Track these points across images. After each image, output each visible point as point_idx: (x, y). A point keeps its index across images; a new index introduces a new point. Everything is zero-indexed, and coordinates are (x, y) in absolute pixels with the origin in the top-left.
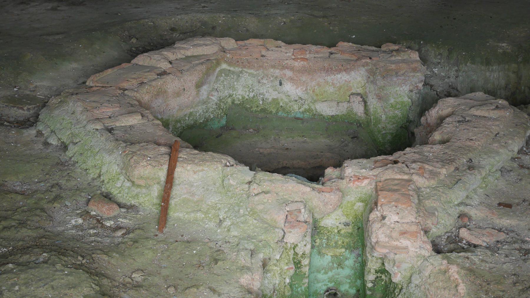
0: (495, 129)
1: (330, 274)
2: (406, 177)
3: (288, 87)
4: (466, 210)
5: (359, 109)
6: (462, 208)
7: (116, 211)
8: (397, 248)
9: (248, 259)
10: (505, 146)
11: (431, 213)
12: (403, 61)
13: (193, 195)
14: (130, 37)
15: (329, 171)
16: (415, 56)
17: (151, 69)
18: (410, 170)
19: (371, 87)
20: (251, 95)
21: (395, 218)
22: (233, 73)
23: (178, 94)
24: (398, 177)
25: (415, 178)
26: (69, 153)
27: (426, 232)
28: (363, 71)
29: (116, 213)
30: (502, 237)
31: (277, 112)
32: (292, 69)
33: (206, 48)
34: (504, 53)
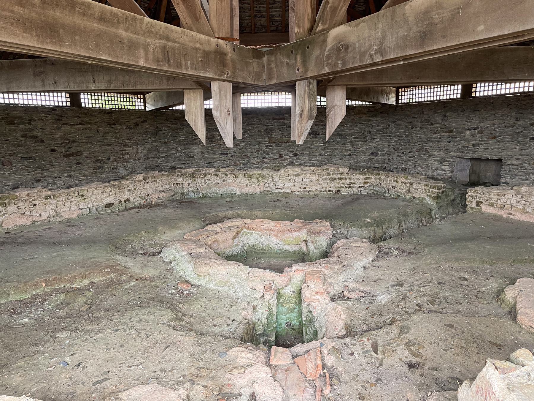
0: (361, 251)
1: (287, 315)
2: (319, 269)
3: (273, 238)
4: (347, 284)
5: (304, 247)
6: (345, 283)
7: (190, 287)
8: (314, 299)
9: (246, 305)
10: (366, 257)
11: (331, 284)
12: (323, 226)
13: (224, 279)
14: (206, 220)
15: (286, 269)
16: (328, 223)
17: (212, 231)
18: (324, 268)
19: (309, 238)
20: (257, 242)
21: (313, 286)
22: (249, 233)
23: (224, 242)
24: (315, 269)
25: (323, 270)
26: (172, 265)
27: (328, 293)
28: (305, 231)
29: (189, 288)
30: (363, 294)
31: (269, 250)
32: (274, 231)
33: (238, 222)
34: (368, 223)
